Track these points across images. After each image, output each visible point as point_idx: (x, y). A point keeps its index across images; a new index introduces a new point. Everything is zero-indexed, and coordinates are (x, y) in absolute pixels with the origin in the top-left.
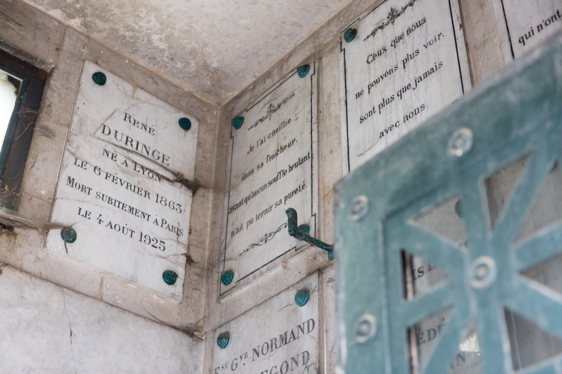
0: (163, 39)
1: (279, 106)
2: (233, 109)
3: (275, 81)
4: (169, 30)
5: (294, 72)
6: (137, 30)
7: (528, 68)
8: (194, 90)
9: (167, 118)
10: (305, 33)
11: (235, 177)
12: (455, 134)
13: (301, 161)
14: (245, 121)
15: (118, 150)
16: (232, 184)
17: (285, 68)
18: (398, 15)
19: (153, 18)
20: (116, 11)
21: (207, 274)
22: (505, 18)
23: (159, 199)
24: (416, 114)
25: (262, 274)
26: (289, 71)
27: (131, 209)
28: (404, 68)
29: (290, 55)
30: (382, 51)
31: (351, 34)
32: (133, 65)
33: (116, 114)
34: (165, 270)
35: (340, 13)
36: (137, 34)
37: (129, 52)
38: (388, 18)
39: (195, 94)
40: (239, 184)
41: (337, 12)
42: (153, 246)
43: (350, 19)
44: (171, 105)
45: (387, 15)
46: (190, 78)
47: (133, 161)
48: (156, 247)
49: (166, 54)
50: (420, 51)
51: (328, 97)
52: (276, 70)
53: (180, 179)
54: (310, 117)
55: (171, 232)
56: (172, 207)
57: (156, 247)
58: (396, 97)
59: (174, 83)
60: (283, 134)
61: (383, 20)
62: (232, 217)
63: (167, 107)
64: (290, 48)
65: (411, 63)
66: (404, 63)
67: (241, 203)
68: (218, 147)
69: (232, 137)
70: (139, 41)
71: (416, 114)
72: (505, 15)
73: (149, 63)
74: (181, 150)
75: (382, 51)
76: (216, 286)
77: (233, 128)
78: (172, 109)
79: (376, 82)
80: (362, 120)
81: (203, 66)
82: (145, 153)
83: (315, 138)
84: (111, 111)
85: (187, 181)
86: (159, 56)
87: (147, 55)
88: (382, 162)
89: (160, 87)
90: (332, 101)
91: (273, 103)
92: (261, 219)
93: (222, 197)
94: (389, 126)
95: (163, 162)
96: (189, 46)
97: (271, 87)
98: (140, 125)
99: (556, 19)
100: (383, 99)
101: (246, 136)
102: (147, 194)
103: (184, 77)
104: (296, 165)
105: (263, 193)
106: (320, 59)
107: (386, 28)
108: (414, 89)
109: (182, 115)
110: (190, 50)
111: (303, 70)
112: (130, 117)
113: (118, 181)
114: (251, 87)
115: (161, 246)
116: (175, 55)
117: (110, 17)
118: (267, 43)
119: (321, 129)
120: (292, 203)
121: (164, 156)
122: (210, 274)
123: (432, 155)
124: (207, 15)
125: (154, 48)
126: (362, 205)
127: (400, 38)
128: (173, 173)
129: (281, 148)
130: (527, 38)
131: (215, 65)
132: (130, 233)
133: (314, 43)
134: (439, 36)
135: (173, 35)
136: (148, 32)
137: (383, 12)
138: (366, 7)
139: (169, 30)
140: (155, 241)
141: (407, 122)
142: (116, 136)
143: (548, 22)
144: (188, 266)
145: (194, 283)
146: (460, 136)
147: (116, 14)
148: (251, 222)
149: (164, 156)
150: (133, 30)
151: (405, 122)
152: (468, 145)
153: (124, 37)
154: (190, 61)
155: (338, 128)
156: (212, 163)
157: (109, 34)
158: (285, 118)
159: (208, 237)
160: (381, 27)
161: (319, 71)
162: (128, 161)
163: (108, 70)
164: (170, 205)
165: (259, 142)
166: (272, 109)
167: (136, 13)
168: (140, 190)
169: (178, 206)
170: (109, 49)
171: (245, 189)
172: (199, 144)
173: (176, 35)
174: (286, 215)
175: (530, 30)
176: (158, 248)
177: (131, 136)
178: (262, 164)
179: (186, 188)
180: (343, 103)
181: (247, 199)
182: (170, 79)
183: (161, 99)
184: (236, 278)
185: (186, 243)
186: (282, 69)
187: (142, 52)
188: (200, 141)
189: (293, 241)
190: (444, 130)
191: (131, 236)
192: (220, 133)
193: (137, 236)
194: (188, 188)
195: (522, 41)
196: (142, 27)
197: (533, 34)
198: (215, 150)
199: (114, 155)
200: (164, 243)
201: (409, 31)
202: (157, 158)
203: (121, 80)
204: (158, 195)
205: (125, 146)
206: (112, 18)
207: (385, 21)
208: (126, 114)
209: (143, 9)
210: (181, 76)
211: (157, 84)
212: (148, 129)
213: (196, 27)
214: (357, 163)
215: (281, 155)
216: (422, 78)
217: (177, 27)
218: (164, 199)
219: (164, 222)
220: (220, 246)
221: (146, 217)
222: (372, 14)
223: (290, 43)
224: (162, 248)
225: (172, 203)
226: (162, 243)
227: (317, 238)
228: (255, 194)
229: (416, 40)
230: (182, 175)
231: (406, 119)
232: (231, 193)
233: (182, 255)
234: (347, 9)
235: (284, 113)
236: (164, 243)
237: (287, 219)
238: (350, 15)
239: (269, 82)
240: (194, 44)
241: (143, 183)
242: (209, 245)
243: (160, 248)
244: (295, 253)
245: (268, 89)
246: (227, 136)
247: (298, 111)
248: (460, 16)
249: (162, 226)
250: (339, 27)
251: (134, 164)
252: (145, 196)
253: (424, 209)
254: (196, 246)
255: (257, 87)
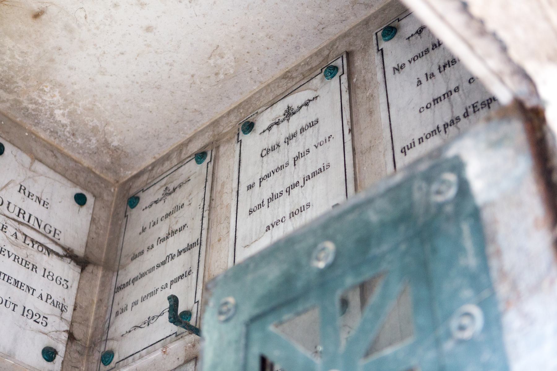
0: (66, 114)
1: (174, 190)
2: (130, 187)
3: (173, 165)
4: (72, 107)
5: (192, 157)
6: (40, 104)
7: (390, 190)
8: (94, 166)
9: (62, 192)
10: (206, 121)
11: (125, 256)
12: (320, 246)
13: (190, 247)
14: (141, 201)
15: (9, 222)
16: (122, 262)
17: (184, 152)
18: (294, 113)
19: (57, 93)
20: (21, 84)
21: (88, 352)
22: (391, 128)
23: (47, 274)
24: (301, 211)
25: (141, 357)
26: (187, 156)
27: (17, 282)
28: (295, 165)
29: (190, 140)
30: (276, 146)
31: (249, 127)
32: (34, 137)
33: (10, 186)
34: (45, 346)
35: (240, 104)
36: (40, 108)
37: (30, 124)
38: (284, 115)
39: (94, 170)
40: (129, 264)
41: (238, 103)
42: (35, 321)
43: (250, 111)
44: (69, 180)
45: (283, 112)
46: (90, 154)
47: (24, 234)
48: (38, 323)
49: (68, 129)
50: (310, 151)
51: (222, 185)
52: (176, 153)
53: (69, 255)
54: (202, 204)
55: (55, 308)
56: (58, 282)
57: (38, 323)
58: (284, 192)
59: (74, 157)
60: (175, 218)
61: (280, 116)
62: (118, 296)
63: (65, 181)
64: (190, 133)
65: (301, 161)
66: (295, 161)
67: (128, 284)
68: (112, 224)
69: (126, 216)
70: (42, 114)
71: (301, 211)
72: (390, 124)
73: (50, 136)
74: (73, 224)
75: (276, 146)
76: (95, 365)
77: (128, 207)
78: (69, 184)
79: (268, 176)
80: (251, 212)
81: (104, 143)
82: (36, 226)
83: (205, 226)
84: (6, 182)
85: (77, 256)
86: (61, 131)
87: (48, 129)
88: (252, 266)
89: (59, 161)
90: (225, 190)
91: (169, 186)
92: (146, 301)
93: (110, 275)
94: (275, 220)
95: (54, 236)
96: (91, 124)
97: (169, 170)
98: (34, 198)
99: (436, 134)
100: (273, 194)
101: (141, 216)
102: (34, 268)
103: (84, 153)
104: (184, 251)
105: (150, 275)
106: (218, 147)
107: (281, 125)
108: (302, 187)
109: (79, 190)
110: (91, 127)
111: (200, 156)
112: (25, 189)
113: (6, 253)
114: (150, 168)
115: (43, 322)
116: (77, 131)
117: (14, 88)
118: (168, 126)
119: (212, 217)
120: (174, 290)
121: (56, 230)
122: (91, 353)
123: (297, 264)
124: (111, 96)
125: (56, 122)
126: (229, 306)
127: (294, 136)
128: (63, 248)
129: (172, 232)
130: (408, 149)
131: (115, 143)
132: (12, 306)
133: (213, 131)
134: (329, 137)
135: (76, 111)
136: (51, 106)
137: (279, 109)
138: (266, 101)
139: (72, 107)
140: (38, 316)
141: (292, 218)
142: (8, 207)
143: (428, 136)
144: (69, 343)
145: (74, 361)
146: (323, 249)
147: (21, 87)
148: (135, 303)
149: (56, 230)
150: (36, 103)
151: (290, 218)
152: (330, 259)
153: (27, 109)
154: (91, 138)
155: (228, 218)
156: (105, 240)
157: (12, 105)
158: (179, 203)
159: (93, 314)
160: (277, 124)
161: (215, 160)
162: (18, 233)
163: (7, 141)
164: (58, 280)
165: (152, 224)
166: (167, 192)
167: (41, 87)
168: (28, 263)
169: (65, 282)
170: (10, 119)
171: (133, 270)
172: (93, 220)
173: (79, 112)
174: (168, 302)
175: (411, 141)
176: (40, 323)
177: (24, 208)
178: (153, 246)
179: (75, 264)
180: (235, 194)
181: (135, 280)
182: (70, 153)
183: (60, 173)
184: (116, 359)
185: (69, 319)
186: (181, 153)
187: (43, 125)
188: (95, 217)
189: (173, 328)
190: (311, 241)
191: (13, 310)
192: (115, 210)
193: (19, 310)
194: (77, 264)
195: (404, 151)
196: (46, 101)
197: (414, 146)
198: (109, 227)
199: (5, 227)
200: (46, 318)
201: (303, 130)
202: (48, 231)
203: (20, 152)
204: (45, 270)
205: (16, 218)
206: (16, 90)
207: (282, 118)
208: (21, 186)
209: (48, 84)
210: (81, 151)
211: (56, 157)
212: (42, 202)
213: (100, 106)
214: (243, 255)
215: (171, 239)
216: (311, 177)
217: (80, 104)
218: (51, 274)
219: (49, 297)
220: (104, 325)
221: (31, 291)
222: (269, 109)
223: (190, 129)
224: (44, 324)
225: (59, 279)
226: (44, 319)
227: (197, 327)
228: (142, 275)
229: (308, 140)
230: (72, 251)
231: (292, 215)
232: (119, 272)
233: (64, 331)
234: (248, 101)
235: (179, 197)
236: (46, 318)
237: (168, 305)
238: (250, 107)
239: (167, 165)
240: (96, 122)
241: (32, 256)
242: (93, 323)
243: (42, 323)
244: (176, 338)
245: (166, 172)
246: (122, 214)
247: (192, 196)
248: (350, 121)
249: (46, 301)
250: (238, 118)
251: (24, 237)
252: (32, 270)
253: (286, 317)
254: (80, 323)
255: (156, 169)
